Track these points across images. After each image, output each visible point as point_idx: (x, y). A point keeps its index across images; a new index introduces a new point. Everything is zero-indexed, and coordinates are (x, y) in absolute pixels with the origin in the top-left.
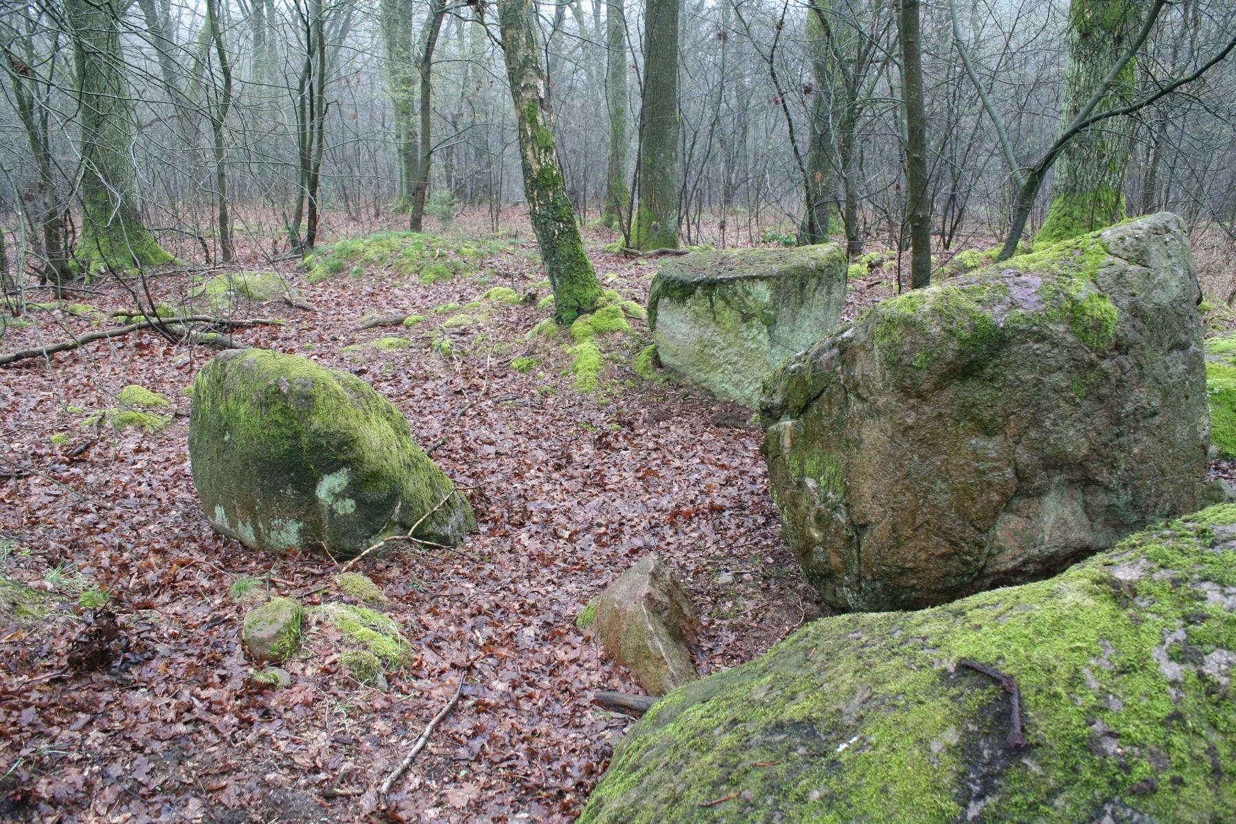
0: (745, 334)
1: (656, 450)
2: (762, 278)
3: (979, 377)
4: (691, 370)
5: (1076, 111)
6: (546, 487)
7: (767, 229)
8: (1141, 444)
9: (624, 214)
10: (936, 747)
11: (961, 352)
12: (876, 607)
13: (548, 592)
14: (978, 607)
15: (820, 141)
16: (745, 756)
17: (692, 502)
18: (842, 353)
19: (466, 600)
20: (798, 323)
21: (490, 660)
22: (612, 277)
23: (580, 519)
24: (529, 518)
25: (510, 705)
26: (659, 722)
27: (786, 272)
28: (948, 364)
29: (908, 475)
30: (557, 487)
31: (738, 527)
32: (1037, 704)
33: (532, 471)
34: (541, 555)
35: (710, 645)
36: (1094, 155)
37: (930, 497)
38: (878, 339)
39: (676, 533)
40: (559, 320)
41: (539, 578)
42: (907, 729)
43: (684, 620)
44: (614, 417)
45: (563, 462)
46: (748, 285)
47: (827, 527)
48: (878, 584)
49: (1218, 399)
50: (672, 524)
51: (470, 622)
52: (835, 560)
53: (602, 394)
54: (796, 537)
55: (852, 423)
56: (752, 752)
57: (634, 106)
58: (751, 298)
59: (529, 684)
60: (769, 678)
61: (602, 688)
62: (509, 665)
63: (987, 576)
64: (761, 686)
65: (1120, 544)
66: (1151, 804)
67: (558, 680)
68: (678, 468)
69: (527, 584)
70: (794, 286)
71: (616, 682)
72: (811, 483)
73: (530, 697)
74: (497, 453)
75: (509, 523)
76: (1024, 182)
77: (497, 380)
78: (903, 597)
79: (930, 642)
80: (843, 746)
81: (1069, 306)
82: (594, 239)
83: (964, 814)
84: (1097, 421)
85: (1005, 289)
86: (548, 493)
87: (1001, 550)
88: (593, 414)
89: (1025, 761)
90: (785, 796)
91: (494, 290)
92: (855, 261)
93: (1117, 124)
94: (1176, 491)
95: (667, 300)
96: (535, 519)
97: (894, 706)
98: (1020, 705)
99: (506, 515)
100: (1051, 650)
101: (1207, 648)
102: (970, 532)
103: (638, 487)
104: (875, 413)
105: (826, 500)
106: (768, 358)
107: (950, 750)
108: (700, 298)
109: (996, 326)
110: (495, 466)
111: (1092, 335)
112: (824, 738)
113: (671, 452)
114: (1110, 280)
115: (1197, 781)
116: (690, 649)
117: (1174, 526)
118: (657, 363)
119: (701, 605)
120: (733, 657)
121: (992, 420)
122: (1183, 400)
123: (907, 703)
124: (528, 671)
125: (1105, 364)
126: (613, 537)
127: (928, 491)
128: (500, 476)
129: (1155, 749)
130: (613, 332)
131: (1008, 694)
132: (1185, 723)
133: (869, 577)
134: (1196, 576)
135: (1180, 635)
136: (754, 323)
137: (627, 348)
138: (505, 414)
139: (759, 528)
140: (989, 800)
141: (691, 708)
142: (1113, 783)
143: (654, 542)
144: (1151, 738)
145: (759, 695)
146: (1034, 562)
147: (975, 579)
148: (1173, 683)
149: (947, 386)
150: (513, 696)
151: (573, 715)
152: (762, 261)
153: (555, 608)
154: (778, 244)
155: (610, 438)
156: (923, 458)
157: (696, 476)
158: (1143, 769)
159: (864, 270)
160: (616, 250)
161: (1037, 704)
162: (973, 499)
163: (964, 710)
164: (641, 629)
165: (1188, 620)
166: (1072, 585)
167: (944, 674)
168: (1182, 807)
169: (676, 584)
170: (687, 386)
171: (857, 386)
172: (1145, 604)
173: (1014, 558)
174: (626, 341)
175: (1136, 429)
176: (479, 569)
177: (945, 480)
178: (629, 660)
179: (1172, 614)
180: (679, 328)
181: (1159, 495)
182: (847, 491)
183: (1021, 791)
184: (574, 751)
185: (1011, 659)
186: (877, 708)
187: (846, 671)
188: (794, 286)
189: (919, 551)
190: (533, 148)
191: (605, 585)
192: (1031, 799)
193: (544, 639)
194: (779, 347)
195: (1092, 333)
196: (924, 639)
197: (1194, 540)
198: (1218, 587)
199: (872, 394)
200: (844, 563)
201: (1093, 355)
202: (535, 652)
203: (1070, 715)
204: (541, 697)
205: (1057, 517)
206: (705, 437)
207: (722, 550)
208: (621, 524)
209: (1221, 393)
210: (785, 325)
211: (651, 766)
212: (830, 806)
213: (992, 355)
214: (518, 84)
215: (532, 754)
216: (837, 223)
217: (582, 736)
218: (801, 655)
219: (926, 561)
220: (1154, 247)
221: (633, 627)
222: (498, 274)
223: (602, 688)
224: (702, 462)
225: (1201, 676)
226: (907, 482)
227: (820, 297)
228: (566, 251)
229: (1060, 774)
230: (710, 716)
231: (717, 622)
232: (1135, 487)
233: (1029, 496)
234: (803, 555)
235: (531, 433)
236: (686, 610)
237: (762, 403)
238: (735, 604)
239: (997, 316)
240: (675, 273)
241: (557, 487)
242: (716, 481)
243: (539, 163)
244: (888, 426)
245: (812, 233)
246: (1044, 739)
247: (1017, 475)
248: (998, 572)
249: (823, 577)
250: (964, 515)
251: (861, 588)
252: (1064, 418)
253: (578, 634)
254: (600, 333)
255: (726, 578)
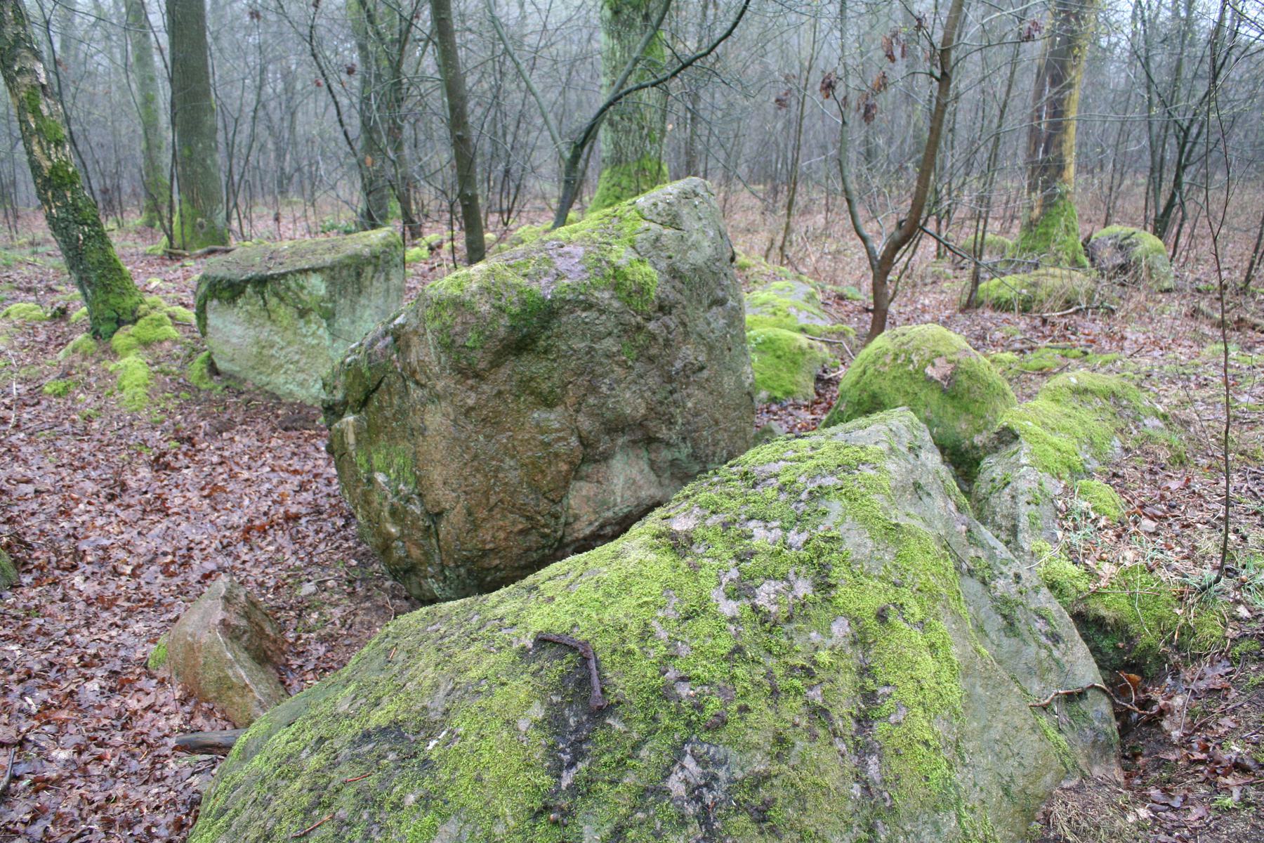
0: (304, 330)
1: (221, 464)
2: (314, 270)
3: (533, 350)
4: (252, 374)
5: (614, 83)
6: (100, 521)
7: (326, 218)
8: (694, 398)
9: (165, 212)
10: (523, 725)
11: (513, 328)
12: (464, 593)
13: (111, 637)
14: (550, 579)
15: (368, 128)
16: (335, 775)
17: (265, 514)
18: (396, 340)
19: (11, 665)
20: (358, 313)
21: (47, 728)
22: (155, 282)
23: (141, 550)
24: (82, 559)
25: (77, 774)
26: (246, 755)
27: (340, 262)
28: (501, 341)
29: (476, 457)
30: (113, 519)
31: (317, 532)
32: (614, 664)
33: (81, 506)
34: (100, 598)
35: (299, 662)
36: (634, 127)
37: (501, 475)
38: (429, 323)
39: (251, 549)
40: (96, 335)
41: (99, 624)
42: (493, 714)
43: (269, 644)
44: (171, 434)
45: (117, 491)
46: (301, 278)
47: (403, 520)
48: (462, 570)
49: (763, 348)
50: (246, 540)
51: (18, 689)
52: (416, 553)
53: (155, 411)
54: (373, 536)
55: (414, 411)
56: (342, 768)
57: (163, 93)
58: (305, 292)
59: (98, 745)
60: (352, 688)
61: (184, 731)
62: (72, 728)
63: (568, 545)
64: (345, 697)
65: (676, 496)
66: (723, 735)
67: (132, 733)
68: (247, 480)
69: (86, 633)
70: (350, 276)
71: (199, 721)
72: (380, 478)
73: (100, 759)
74: (36, 491)
75: (58, 568)
76: (568, 155)
77: (28, 409)
78: (489, 579)
79: (507, 622)
80: (432, 744)
81: (612, 272)
82: (127, 238)
83: (558, 785)
84: (651, 382)
85: (549, 261)
86: (102, 528)
87: (577, 518)
88: (147, 434)
89: (608, 721)
90: (381, 807)
91: (14, 308)
92: (414, 245)
93: (650, 96)
94: (731, 438)
95: (215, 302)
96: (89, 559)
97: (478, 692)
98: (597, 669)
99: (54, 559)
100: (617, 612)
101: (758, 581)
102: (544, 505)
103: (205, 506)
104: (436, 397)
105: (398, 493)
106: (331, 353)
107: (537, 725)
108: (251, 297)
109: (544, 298)
110: (35, 506)
111: (636, 300)
112: (413, 739)
113: (237, 464)
114: (647, 245)
115: (759, 703)
116: (278, 670)
117: (721, 473)
118: (213, 370)
119: (284, 622)
120: (325, 670)
121: (551, 392)
122: (726, 352)
123: (491, 687)
124: (95, 730)
125: (652, 326)
126: (181, 565)
127: (498, 469)
128: (42, 517)
129: (722, 685)
130: (160, 342)
131: (585, 660)
132: (745, 654)
133: (452, 565)
134: (743, 517)
135: (734, 574)
136: (312, 317)
137: (178, 357)
138: (42, 446)
139: (339, 531)
140: (580, 765)
141: (277, 735)
142: (689, 724)
143: (228, 562)
144: (718, 674)
145: (343, 707)
146: (611, 524)
147: (556, 550)
148: (732, 620)
149: (503, 363)
150: (81, 763)
151: (153, 768)
152: (314, 252)
153: (122, 653)
154: (338, 233)
155: (169, 458)
156: (488, 438)
157: (267, 486)
158: (714, 705)
159: (425, 253)
160: (160, 252)
161: (614, 664)
162: (542, 472)
163: (546, 684)
164: (219, 659)
165: (740, 558)
166: (635, 545)
167: (523, 651)
168: (749, 731)
169: (254, 604)
170: (248, 392)
171: (414, 373)
172: (702, 549)
173: (591, 524)
174: (176, 350)
175: (687, 385)
176: (25, 626)
177: (513, 457)
178: (211, 695)
179: (725, 556)
180: (232, 331)
181: (716, 444)
182: (418, 480)
183: (608, 750)
184: (158, 808)
185: (584, 625)
186: (462, 698)
187: (427, 666)
188: (350, 276)
189: (498, 531)
190: (39, 142)
191: (178, 618)
192: (619, 756)
193: (112, 690)
194: (341, 341)
195: (636, 298)
196: (501, 619)
197: (739, 483)
198: (762, 524)
199: (430, 379)
200: (425, 554)
201: (639, 318)
202: (101, 707)
203: (645, 668)
204: (113, 756)
205: (625, 476)
206: (274, 443)
207: (302, 560)
208: (190, 549)
209: (764, 342)
210: (345, 316)
211: (239, 806)
212: (426, 807)
213: (543, 327)
214: (10, 67)
215: (108, 823)
216: (395, 207)
217: (165, 789)
218: (382, 657)
219: (505, 539)
220: (685, 211)
221: (211, 659)
222: (19, 289)
223: (184, 731)
224: (273, 470)
225: (755, 608)
226: (476, 463)
227: (378, 285)
228: (95, 257)
229: (642, 726)
230: (296, 740)
231: (305, 636)
232: (693, 440)
233: (596, 461)
234: (383, 552)
235: (76, 463)
236: (268, 630)
237: (323, 401)
238: (321, 614)
239: (545, 289)
240: (222, 273)
241: (113, 519)
242: (289, 488)
243: (49, 158)
244: (450, 410)
245: (371, 220)
246: (623, 696)
247: (581, 442)
248: (577, 540)
249: (406, 571)
250: (535, 488)
251: (445, 577)
252: (619, 382)
253: (151, 676)
254: (146, 344)
255: (308, 588)
